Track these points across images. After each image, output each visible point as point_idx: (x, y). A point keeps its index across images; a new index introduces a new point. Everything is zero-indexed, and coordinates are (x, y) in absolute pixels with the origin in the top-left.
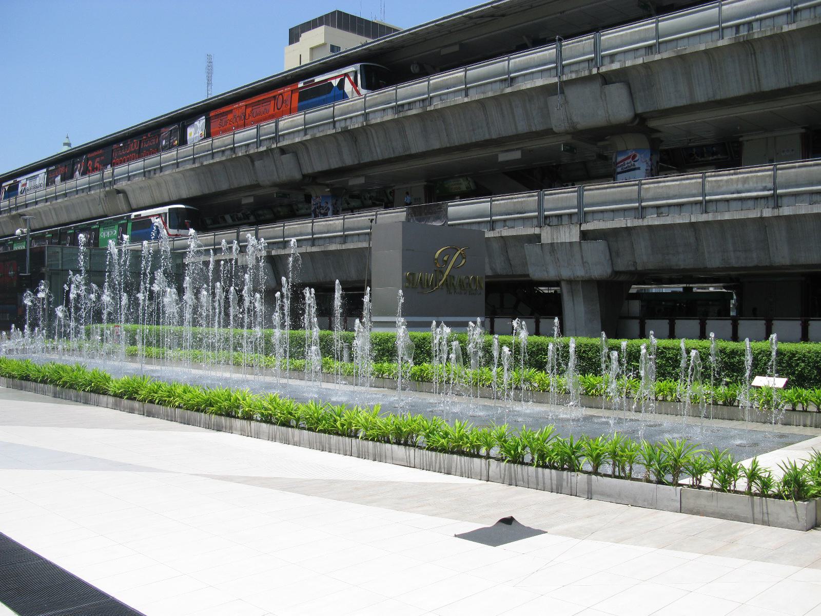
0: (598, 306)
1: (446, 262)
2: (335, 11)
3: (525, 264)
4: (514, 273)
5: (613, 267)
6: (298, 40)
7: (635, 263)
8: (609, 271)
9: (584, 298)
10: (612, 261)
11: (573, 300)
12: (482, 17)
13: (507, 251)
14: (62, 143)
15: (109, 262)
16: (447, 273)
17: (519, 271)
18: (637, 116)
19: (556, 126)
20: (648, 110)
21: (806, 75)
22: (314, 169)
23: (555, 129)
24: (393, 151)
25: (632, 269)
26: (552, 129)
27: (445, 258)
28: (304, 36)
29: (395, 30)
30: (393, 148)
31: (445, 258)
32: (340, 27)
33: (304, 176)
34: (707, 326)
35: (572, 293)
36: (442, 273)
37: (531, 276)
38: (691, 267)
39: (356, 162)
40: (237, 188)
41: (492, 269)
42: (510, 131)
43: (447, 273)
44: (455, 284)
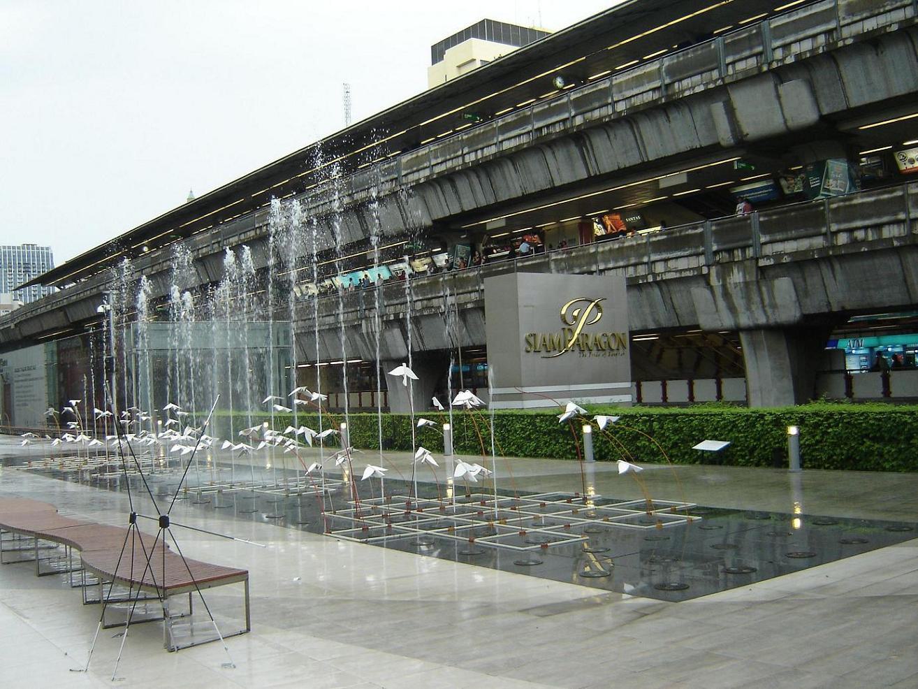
0: (788, 360)
1: (575, 318)
2: (484, 20)
3: (694, 313)
4: (683, 325)
5: (801, 309)
6: (442, 58)
7: (829, 303)
8: (798, 315)
9: (769, 350)
10: (799, 303)
11: (756, 354)
12: (630, 13)
13: (671, 298)
14: (456, 68)
15: (595, 253)
16: (578, 331)
17: (686, 321)
18: (822, 118)
19: (723, 139)
20: (835, 110)
21: (900, 87)
22: (444, 213)
23: (723, 143)
24: (535, 186)
25: (825, 310)
26: (719, 143)
27: (575, 313)
28: (449, 53)
29: (548, 33)
30: (534, 182)
31: (575, 313)
32: (490, 39)
33: (434, 221)
34: (688, 395)
35: (755, 346)
36: (572, 332)
37: (701, 326)
38: (900, 304)
39: (493, 202)
40: (437, 220)
41: (655, 321)
42: (671, 150)
43: (578, 331)
44: (590, 344)
